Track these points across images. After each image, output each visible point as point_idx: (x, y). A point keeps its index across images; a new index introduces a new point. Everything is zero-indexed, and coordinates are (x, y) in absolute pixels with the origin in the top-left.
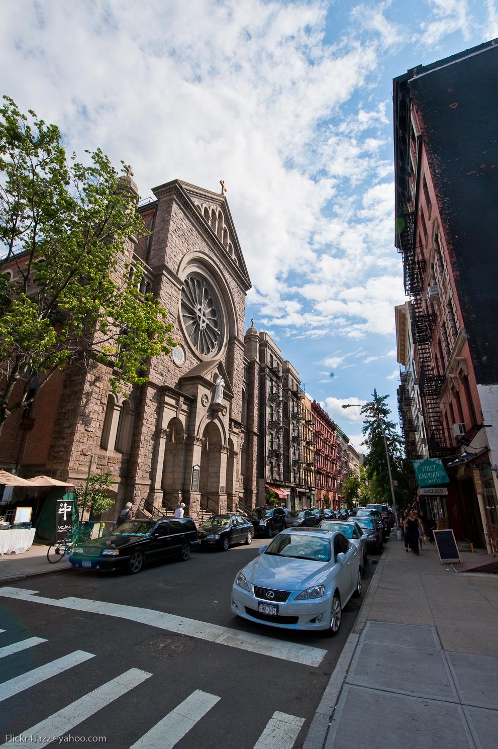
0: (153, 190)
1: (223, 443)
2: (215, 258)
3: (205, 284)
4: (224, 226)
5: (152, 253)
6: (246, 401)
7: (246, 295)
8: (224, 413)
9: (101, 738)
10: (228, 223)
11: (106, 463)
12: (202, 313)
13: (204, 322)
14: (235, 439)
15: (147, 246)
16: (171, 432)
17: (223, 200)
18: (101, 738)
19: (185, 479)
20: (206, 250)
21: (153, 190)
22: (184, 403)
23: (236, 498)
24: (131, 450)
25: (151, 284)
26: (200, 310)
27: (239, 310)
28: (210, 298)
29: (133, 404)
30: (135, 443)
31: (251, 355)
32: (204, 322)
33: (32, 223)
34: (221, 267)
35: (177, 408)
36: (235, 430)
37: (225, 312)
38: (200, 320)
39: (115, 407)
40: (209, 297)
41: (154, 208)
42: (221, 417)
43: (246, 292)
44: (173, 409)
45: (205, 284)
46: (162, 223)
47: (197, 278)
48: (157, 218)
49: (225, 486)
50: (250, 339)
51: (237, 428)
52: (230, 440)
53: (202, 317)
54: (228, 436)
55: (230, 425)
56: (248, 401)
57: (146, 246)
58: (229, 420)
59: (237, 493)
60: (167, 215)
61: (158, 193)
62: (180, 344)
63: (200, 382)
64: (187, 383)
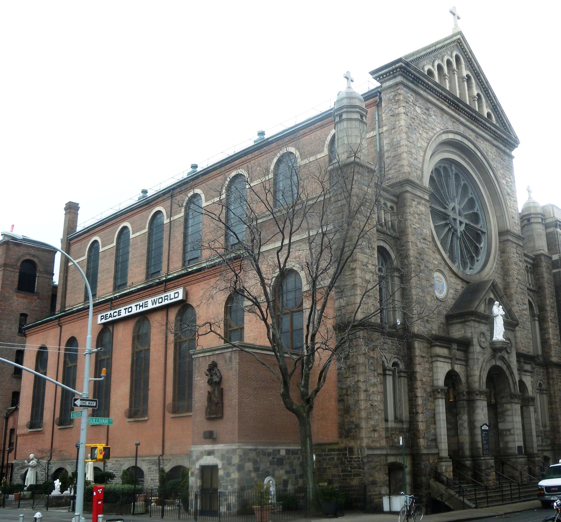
0: (372, 73)
1: (513, 391)
2: (462, 129)
3: (453, 168)
4: (465, 73)
6: (536, 318)
9: (98, 422)
10: (471, 64)
11: (390, 435)
12: (457, 212)
13: (461, 223)
14: (528, 380)
15: (378, 150)
16: (448, 390)
17: (459, 36)
18: (98, 422)
19: (467, 371)
20: (450, 126)
21: (372, 73)
22: (458, 350)
23: (540, 459)
24: (410, 417)
26: (454, 209)
28: (464, 184)
29: (403, 363)
30: (413, 408)
32: (461, 223)
33: (321, 298)
34: (472, 136)
35: (451, 359)
36: (528, 367)
37: (488, 197)
38: (455, 224)
40: (462, 183)
41: (377, 95)
42: (506, 356)
44: (447, 360)
45: (453, 168)
46: (392, 118)
48: (383, 111)
49: (522, 445)
50: (529, 220)
51: (530, 364)
52: (522, 384)
53: (459, 218)
54: (517, 379)
55: (518, 361)
56: (539, 317)
57: (376, 150)
58: (517, 355)
59: (540, 452)
60: (397, 107)
61: (379, 77)
62: (439, 270)
63: (473, 318)
64: (455, 321)
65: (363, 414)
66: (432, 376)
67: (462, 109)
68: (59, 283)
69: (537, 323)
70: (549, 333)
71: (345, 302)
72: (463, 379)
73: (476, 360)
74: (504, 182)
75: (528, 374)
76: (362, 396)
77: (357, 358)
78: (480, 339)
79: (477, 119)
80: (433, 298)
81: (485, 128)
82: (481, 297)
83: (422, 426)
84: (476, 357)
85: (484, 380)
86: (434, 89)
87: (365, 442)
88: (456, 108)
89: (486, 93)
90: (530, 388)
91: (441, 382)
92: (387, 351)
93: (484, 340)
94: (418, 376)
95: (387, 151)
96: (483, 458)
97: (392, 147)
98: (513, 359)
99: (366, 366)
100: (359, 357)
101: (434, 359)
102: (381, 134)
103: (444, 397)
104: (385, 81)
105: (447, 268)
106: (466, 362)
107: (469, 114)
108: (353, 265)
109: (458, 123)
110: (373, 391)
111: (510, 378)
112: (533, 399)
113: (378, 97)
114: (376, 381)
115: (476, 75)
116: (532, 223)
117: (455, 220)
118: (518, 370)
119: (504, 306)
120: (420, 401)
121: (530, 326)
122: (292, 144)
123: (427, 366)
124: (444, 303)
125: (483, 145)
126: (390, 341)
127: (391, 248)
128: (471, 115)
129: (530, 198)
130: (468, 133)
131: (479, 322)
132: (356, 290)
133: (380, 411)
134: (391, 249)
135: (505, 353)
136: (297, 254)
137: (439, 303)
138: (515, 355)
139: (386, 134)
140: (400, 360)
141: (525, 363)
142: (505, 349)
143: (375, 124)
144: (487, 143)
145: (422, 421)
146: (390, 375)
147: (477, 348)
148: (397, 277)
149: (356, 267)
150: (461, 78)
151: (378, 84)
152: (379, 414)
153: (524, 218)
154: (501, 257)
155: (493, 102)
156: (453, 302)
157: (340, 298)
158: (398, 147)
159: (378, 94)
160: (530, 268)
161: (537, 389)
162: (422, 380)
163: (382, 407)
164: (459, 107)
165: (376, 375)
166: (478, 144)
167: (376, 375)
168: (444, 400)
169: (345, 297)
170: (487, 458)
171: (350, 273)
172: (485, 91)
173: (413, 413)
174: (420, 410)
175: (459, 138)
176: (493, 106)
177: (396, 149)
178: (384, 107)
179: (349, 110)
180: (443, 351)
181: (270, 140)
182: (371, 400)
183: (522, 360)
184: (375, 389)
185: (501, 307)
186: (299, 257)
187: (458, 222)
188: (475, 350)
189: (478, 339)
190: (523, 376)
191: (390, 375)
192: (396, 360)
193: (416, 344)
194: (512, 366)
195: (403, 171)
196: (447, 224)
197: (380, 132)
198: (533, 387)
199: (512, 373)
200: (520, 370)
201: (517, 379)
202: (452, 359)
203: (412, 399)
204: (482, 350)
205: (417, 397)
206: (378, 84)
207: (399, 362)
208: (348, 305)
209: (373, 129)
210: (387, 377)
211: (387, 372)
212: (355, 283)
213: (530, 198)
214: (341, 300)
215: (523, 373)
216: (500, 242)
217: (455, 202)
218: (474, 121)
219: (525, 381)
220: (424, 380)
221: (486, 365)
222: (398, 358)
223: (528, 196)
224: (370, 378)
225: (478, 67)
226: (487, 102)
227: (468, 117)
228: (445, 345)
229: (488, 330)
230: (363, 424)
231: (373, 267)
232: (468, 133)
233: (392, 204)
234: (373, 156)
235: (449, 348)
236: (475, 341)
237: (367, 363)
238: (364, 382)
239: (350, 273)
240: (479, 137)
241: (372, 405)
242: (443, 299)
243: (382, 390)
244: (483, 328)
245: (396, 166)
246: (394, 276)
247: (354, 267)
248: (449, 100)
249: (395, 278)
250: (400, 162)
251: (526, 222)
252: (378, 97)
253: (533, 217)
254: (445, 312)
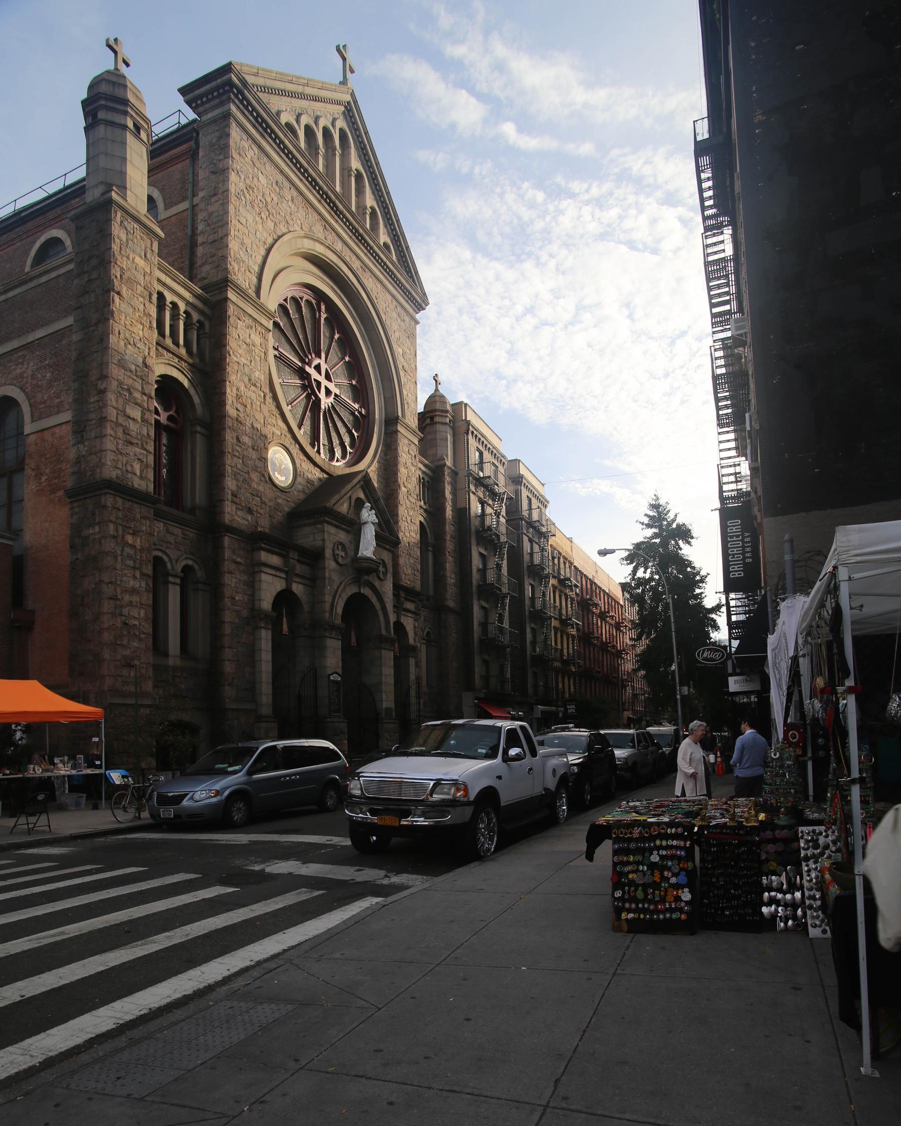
2: (339, 246)
5: (200, 251)
6: (430, 548)
7: (417, 322)
8: (381, 576)
14: (409, 623)
20: (319, 230)
21: (184, 91)
22: (299, 561)
25: (207, 324)
27: (402, 360)
31: (436, 453)
34: (356, 265)
35: (286, 573)
36: (410, 606)
37: (373, 366)
39: (171, 579)
42: (377, 584)
43: (418, 316)
44: (279, 574)
47: (306, 297)
50: (432, 418)
51: (413, 602)
53: (324, 383)
54: (392, 618)
55: (396, 595)
57: (186, 234)
60: (221, 157)
65: (107, 637)
66: (253, 595)
67: (341, 213)
68: (168, 590)
69: (430, 555)
70: (446, 569)
71: (86, 449)
72: (306, 607)
73: (327, 581)
74: (400, 351)
75: (409, 615)
76: (107, 606)
77: (100, 543)
78: (337, 552)
79: (366, 241)
80: (263, 479)
81: (378, 261)
82: (343, 492)
83: (228, 668)
84: (327, 575)
85: (340, 610)
86: (294, 156)
87: (108, 682)
88: (332, 209)
89: (385, 211)
90: (411, 634)
91: (266, 604)
92: (172, 547)
93: (343, 554)
94: (227, 592)
95: (202, 232)
96: (329, 720)
97: (209, 225)
98: (387, 588)
99: (116, 558)
100: (103, 541)
101: (257, 569)
102: (196, 208)
103: (270, 627)
104: (206, 112)
105: (297, 446)
106: (314, 581)
107: (354, 227)
108: (101, 384)
109: (334, 234)
110: (131, 602)
111: (380, 613)
112: (414, 649)
113: (193, 142)
114: (138, 586)
115: (372, 177)
116: (436, 423)
117: (319, 384)
118: (394, 606)
119: (379, 511)
120: (227, 629)
121: (419, 554)
122: (58, 224)
123: (245, 578)
124: (287, 494)
125: (370, 283)
126: (180, 531)
127: (194, 386)
128: (357, 231)
129: (437, 390)
130: (347, 255)
131: (337, 527)
132: (105, 427)
133: (143, 636)
134: (192, 388)
135: (376, 578)
136: (18, 371)
137: (279, 494)
138: (391, 585)
139: (202, 206)
140: (198, 564)
141: (407, 599)
142: (376, 571)
143: (187, 190)
144: (379, 286)
145: (229, 660)
146: (175, 584)
147: (330, 564)
148: (201, 434)
149: (106, 388)
150: (346, 170)
151: (192, 115)
152: (140, 640)
153: (427, 415)
154: (386, 454)
155: (395, 229)
156: (302, 496)
157: (79, 443)
158: (218, 227)
159: (194, 135)
160: (428, 482)
161: (423, 639)
162: (234, 599)
163: (148, 628)
165: (138, 576)
166: (365, 281)
167: (138, 576)
168: (270, 633)
169: (88, 439)
170: (334, 720)
171: (96, 398)
172: (384, 208)
173: (216, 646)
174: (227, 641)
175: (334, 258)
176: (394, 236)
177: (216, 230)
178: (203, 156)
179: (110, 104)
180: (275, 560)
181: (24, 214)
182: (125, 616)
183: (402, 594)
184: (135, 599)
185: (373, 511)
186: (21, 376)
187: (323, 390)
188: (326, 566)
189: (333, 550)
190: (402, 617)
191: (175, 584)
192: (190, 563)
193: (227, 541)
194: (386, 600)
195: (224, 266)
197: (194, 204)
198: (416, 634)
199: (384, 608)
200: (398, 607)
201: (392, 618)
202: (289, 574)
203: (216, 623)
204: (338, 567)
205: (223, 622)
206: (192, 115)
207: (196, 567)
208: (91, 454)
209: (184, 199)
210: (171, 587)
211: (171, 579)
212: (104, 416)
213: (437, 390)
214: (81, 446)
215: (403, 613)
216: (386, 433)
217: (320, 357)
218: (360, 241)
219: (405, 624)
220: (237, 598)
221: (344, 589)
222: (194, 561)
223: (434, 388)
224: (125, 579)
225: (376, 164)
226: (386, 226)
228: (276, 550)
229: (351, 542)
230: (107, 654)
231: (145, 398)
232: (347, 255)
233: (202, 319)
234: (182, 244)
235: (285, 557)
236: (328, 553)
237: (119, 552)
238: (110, 583)
239: (96, 398)
241: (125, 624)
242: (284, 488)
243: (151, 602)
244: (342, 536)
245: (215, 258)
246: (196, 432)
247: (103, 387)
248: (321, 188)
249: (198, 435)
250: (221, 251)
251: (428, 421)
252: (193, 142)
253: (439, 415)
254: (287, 509)
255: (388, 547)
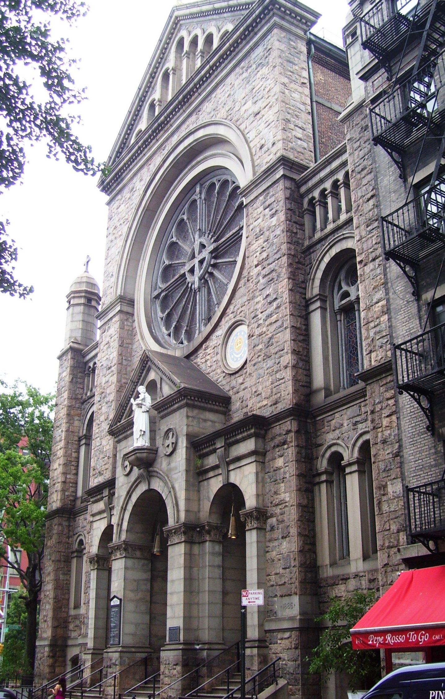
53: (196, 261)
67: (166, 118)
75: (244, 462)
107: (177, 106)
128: (180, 103)
164: (163, 122)
196: (211, 274)
227: (179, 109)
240: (198, 109)
255: (176, 406)
